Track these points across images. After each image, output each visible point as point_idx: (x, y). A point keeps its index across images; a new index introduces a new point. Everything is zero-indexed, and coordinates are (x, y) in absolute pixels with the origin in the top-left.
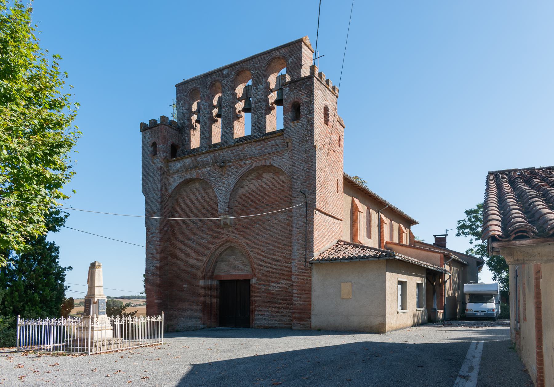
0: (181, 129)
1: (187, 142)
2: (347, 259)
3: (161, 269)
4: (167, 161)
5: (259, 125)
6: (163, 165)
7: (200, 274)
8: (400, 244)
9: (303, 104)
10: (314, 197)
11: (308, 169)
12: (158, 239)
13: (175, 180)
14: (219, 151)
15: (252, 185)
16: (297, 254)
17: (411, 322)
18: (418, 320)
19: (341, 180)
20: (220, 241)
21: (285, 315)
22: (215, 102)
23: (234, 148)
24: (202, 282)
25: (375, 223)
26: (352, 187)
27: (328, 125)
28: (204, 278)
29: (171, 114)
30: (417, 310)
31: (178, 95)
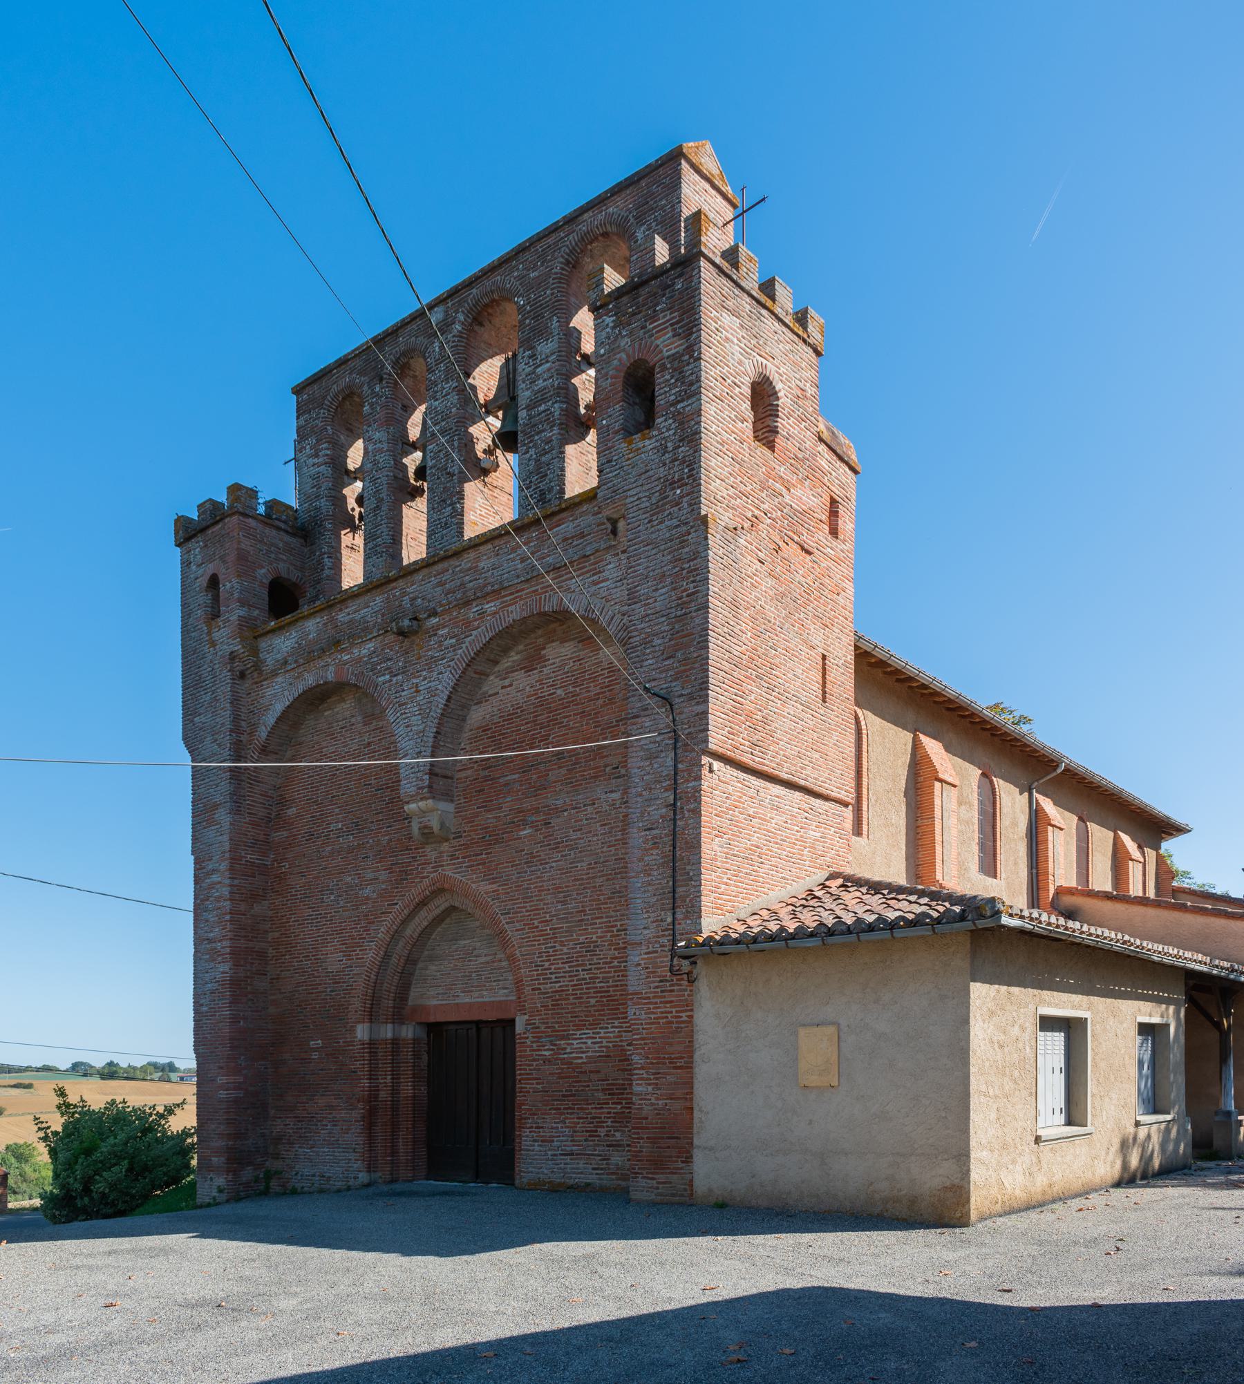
0: (309, 531)
1: (327, 572)
2: (812, 935)
3: (238, 989)
4: (252, 634)
5: (541, 486)
6: (237, 647)
7: (357, 1004)
8: (1119, 896)
9: (663, 368)
10: (700, 708)
11: (681, 606)
12: (226, 891)
13: (278, 696)
14: (401, 583)
15: (511, 689)
16: (644, 925)
17: (1109, 1168)
18: (1146, 1160)
19: (843, 657)
20: (416, 890)
21: (616, 1145)
22: (414, 432)
23: (445, 564)
24: (362, 1032)
25: (1014, 824)
26: (887, 683)
27: (771, 446)
28: (372, 1015)
29: (280, 485)
30: (1137, 1124)
31: (302, 422)
